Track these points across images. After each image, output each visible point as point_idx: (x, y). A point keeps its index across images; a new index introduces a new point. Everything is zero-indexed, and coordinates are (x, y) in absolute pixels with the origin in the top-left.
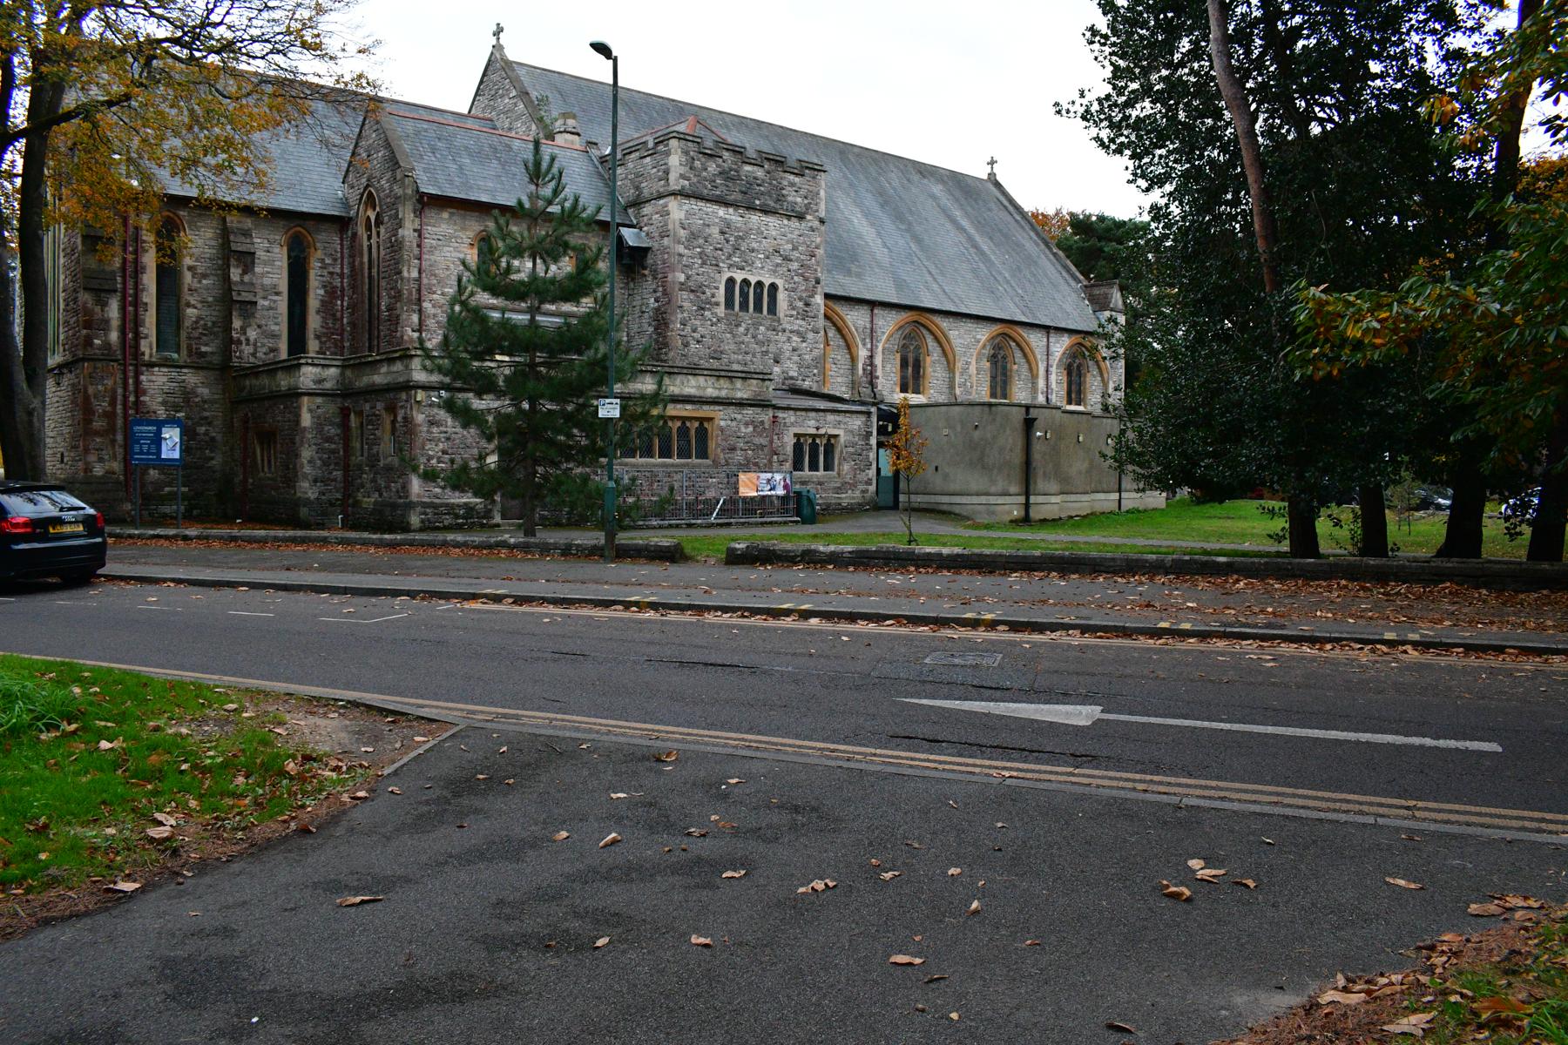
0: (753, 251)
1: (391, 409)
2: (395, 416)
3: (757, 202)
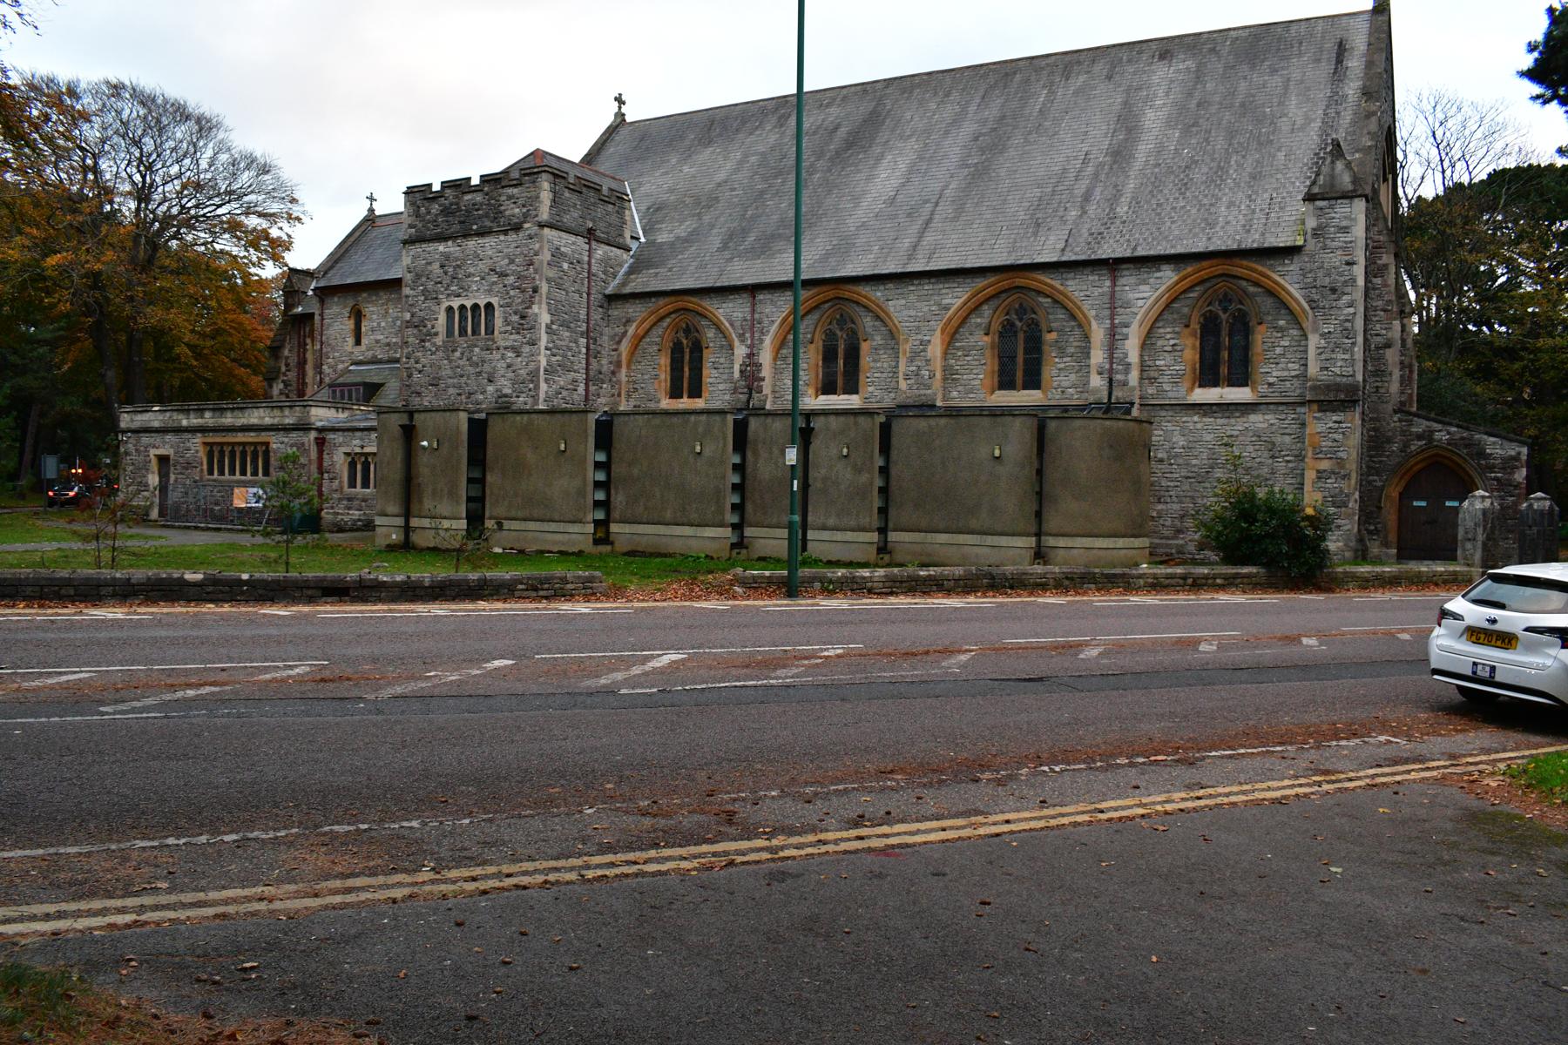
3: (475, 227)
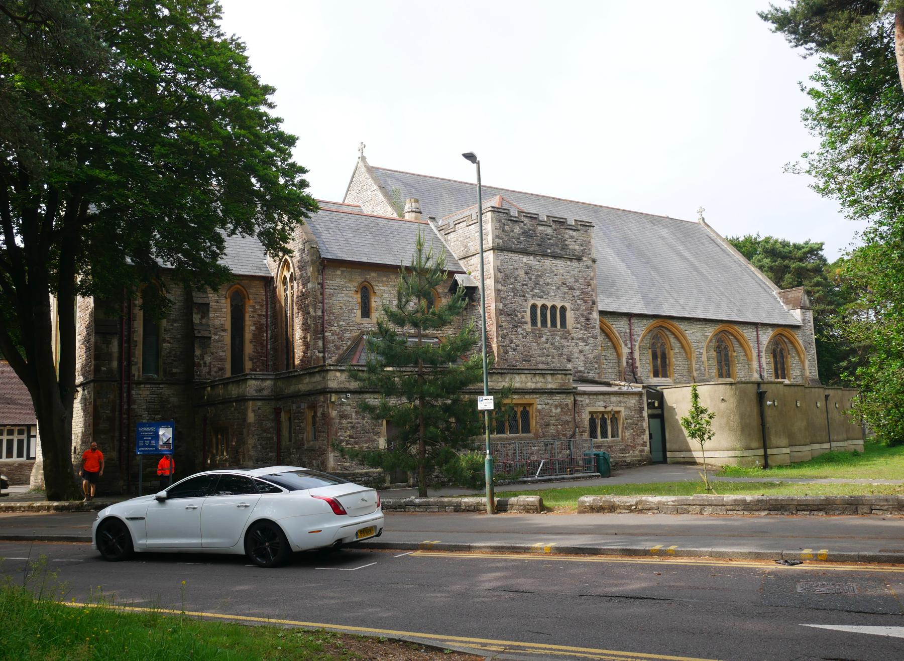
0: (548, 284)
1: (313, 407)
2: (315, 413)
3: (549, 251)
